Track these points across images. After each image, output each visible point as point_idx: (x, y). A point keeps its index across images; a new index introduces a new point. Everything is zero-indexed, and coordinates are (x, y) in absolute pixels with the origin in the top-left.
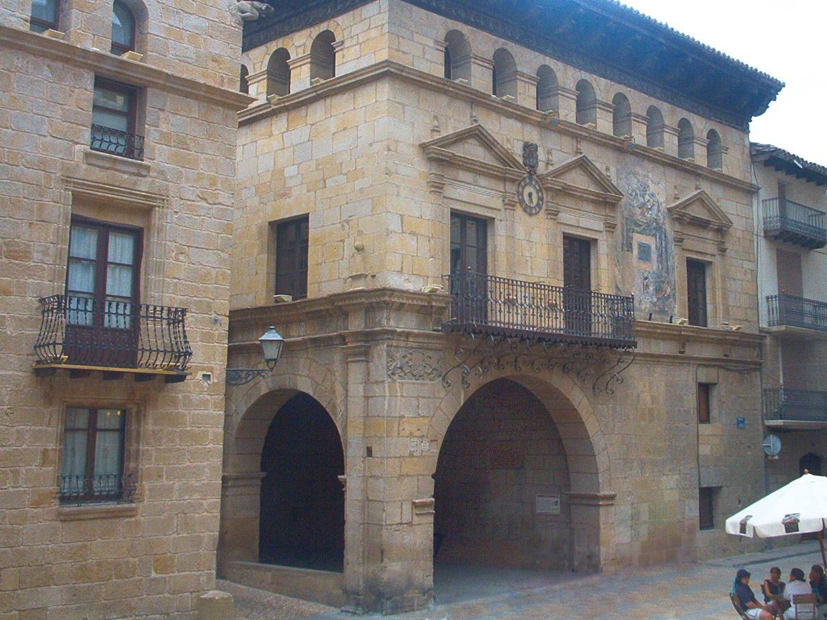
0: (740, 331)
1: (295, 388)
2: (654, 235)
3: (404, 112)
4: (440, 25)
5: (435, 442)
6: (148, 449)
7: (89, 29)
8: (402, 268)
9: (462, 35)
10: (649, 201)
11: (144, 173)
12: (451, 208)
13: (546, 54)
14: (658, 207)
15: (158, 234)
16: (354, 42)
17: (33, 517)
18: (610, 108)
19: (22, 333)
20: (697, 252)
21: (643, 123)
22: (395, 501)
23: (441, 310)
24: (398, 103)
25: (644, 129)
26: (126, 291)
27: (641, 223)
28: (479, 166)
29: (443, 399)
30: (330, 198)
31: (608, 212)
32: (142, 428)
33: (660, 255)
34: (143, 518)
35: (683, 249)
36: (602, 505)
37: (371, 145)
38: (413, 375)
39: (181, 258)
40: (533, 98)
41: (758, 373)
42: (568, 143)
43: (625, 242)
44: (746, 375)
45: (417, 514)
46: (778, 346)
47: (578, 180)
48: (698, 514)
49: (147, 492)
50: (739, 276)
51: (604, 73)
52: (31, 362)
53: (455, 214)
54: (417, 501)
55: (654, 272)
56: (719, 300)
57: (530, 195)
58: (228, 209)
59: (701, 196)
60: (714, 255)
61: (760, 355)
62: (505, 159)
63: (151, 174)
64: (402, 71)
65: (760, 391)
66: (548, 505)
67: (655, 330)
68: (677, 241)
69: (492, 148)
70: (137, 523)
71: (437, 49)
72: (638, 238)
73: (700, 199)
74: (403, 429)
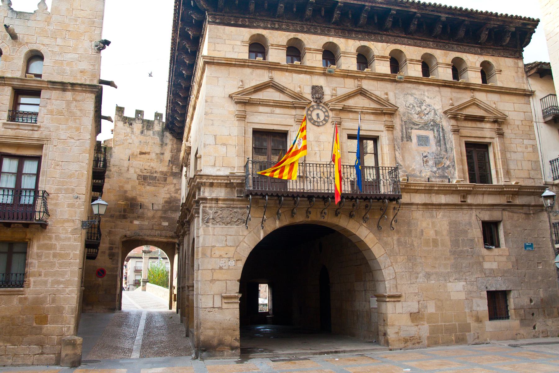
0: (519, 184)
2: (433, 130)
3: (218, 81)
8: (215, 164)
9: (263, 36)
10: (425, 109)
11: (36, 129)
13: (330, 36)
14: (435, 112)
22: (208, 295)
24: (213, 77)
29: (245, 236)
31: (386, 118)
36: (388, 301)
39: (58, 167)
43: (404, 136)
48: (486, 308)
50: (519, 149)
53: (468, 144)
57: (318, 115)
60: (494, 138)
62: (298, 96)
63: (41, 129)
64: (214, 60)
67: (433, 188)
72: (415, 133)
73: (474, 103)
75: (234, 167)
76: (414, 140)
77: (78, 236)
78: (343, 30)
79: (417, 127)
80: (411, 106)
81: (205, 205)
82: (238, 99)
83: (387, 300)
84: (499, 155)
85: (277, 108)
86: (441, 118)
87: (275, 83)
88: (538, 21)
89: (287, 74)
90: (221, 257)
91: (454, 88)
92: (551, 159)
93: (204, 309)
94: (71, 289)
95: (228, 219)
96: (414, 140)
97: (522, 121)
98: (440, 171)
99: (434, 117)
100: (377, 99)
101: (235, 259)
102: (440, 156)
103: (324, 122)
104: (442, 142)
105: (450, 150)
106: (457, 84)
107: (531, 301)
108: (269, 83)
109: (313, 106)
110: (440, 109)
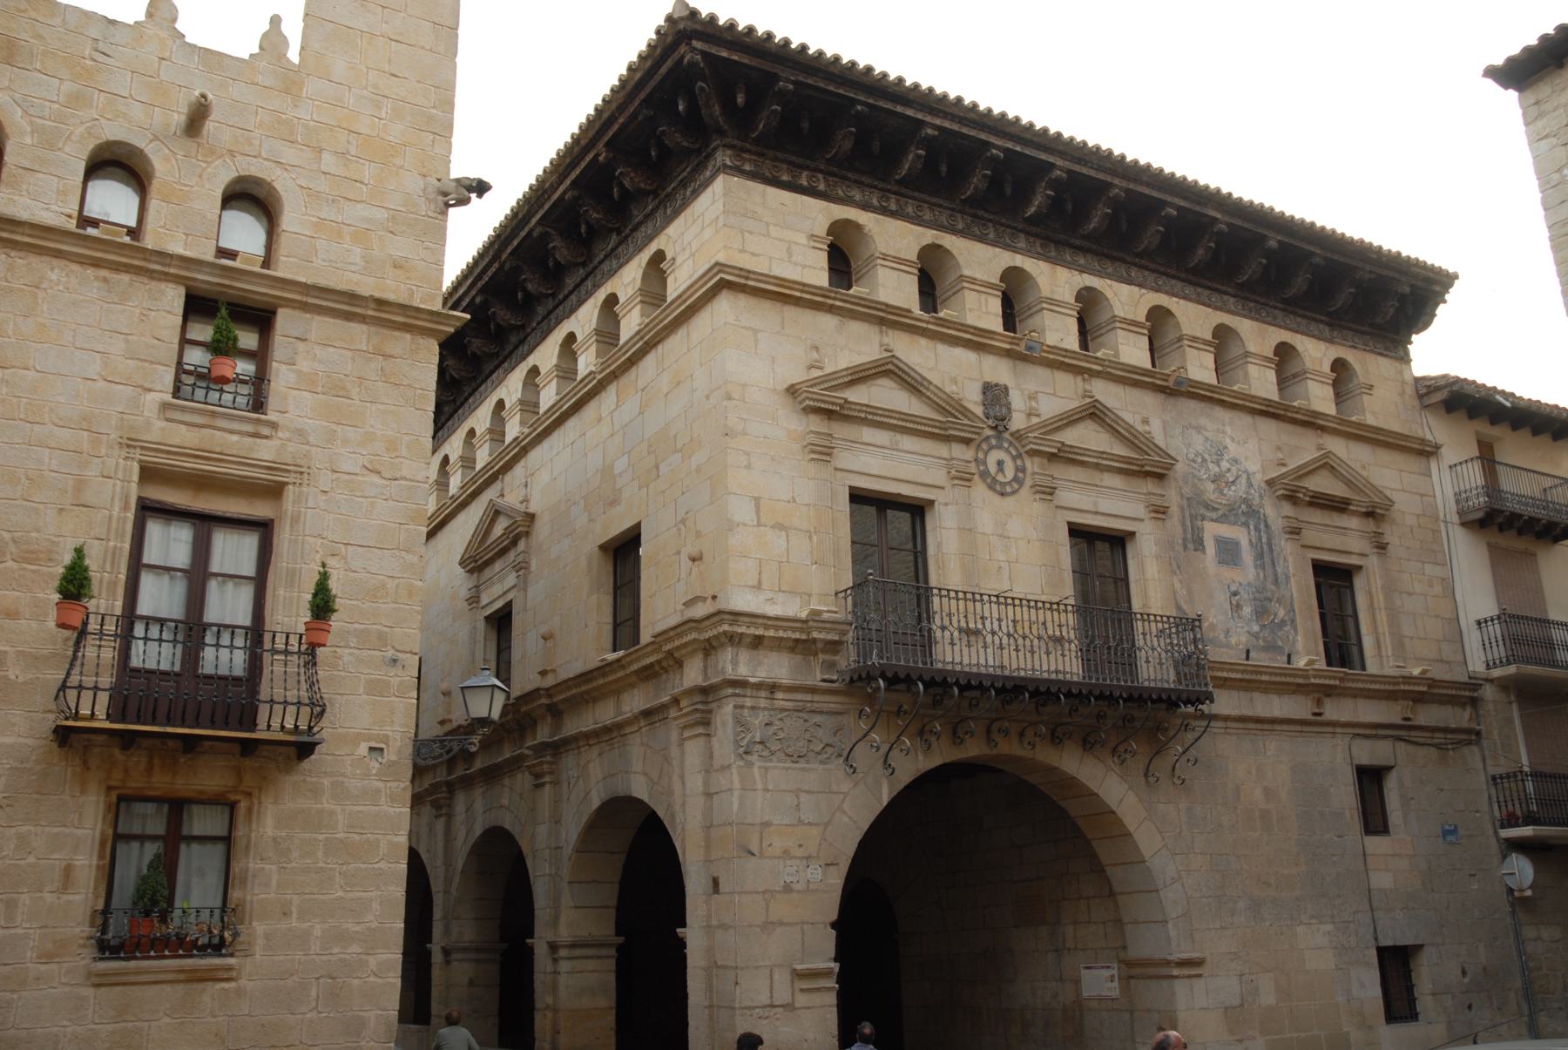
0: (1428, 675)
1: (629, 793)
2: (1246, 525)
3: (756, 341)
4: (818, 214)
5: (836, 867)
6: (263, 869)
7: (178, 227)
10: (1229, 470)
11: (266, 431)
12: (850, 487)
13: (1015, 250)
14: (1248, 479)
15: (292, 526)
16: (687, 254)
17: (38, 979)
18: (1142, 328)
19: (38, 678)
20: (1330, 550)
21: (1206, 350)
22: (757, 967)
23: (834, 646)
24: (743, 328)
25: (1209, 359)
26: (244, 617)
27: (1216, 506)
28: (899, 419)
29: (846, 794)
30: (663, 492)
31: (1150, 486)
32: (253, 834)
33: (1260, 556)
34: (252, 983)
35: (1303, 546)
36: (1177, 977)
37: (708, 397)
38: (787, 755)
40: (996, 315)
41: (1475, 749)
42: (1065, 381)
43: (1189, 536)
44: (1451, 752)
45: (802, 990)
46: (1510, 703)
47: (1087, 437)
49: (260, 941)
50: (1418, 588)
51: (1125, 274)
52: (51, 721)
53: (858, 497)
54: (799, 967)
55: (1249, 584)
56: (1384, 627)
57: (1000, 463)
58: (419, 487)
59: (1327, 460)
61: (1476, 717)
62: (950, 407)
63: (280, 434)
65: (1483, 779)
66: (1100, 982)
68: (1291, 533)
69: (920, 391)
70: (240, 992)
71: (814, 247)
72: (1212, 530)
73: (1326, 464)
74: (770, 845)
75: (810, 595)
76: (1211, 549)
77: (402, 785)
78: (1047, 240)
79: (1214, 515)
80: (1199, 460)
81: (740, 701)
82: (814, 400)
83: (1175, 972)
84: (1380, 599)
85: (905, 436)
86: (1261, 496)
87: (901, 365)
88: (1456, 276)
89: (923, 342)
90: (786, 854)
91: (1284, 421)
92: (1481, 617)
93: (748, 1012)
94: (384, 957)
95: (801, 744)
96: (1211, 549)
97: (1418, 516)
98: (1266, 633)
99: (1247, 493)
100: (1130, 433)
101: (822, 863)
102: (1265, 594)
103: (1016, 486)
104: (1267, 559)
105: (1284, 581)
106: (1292, 412)
107: (1464, 973)
108: (887, 364)
109: (987, 439)
110: (1258, 472)
